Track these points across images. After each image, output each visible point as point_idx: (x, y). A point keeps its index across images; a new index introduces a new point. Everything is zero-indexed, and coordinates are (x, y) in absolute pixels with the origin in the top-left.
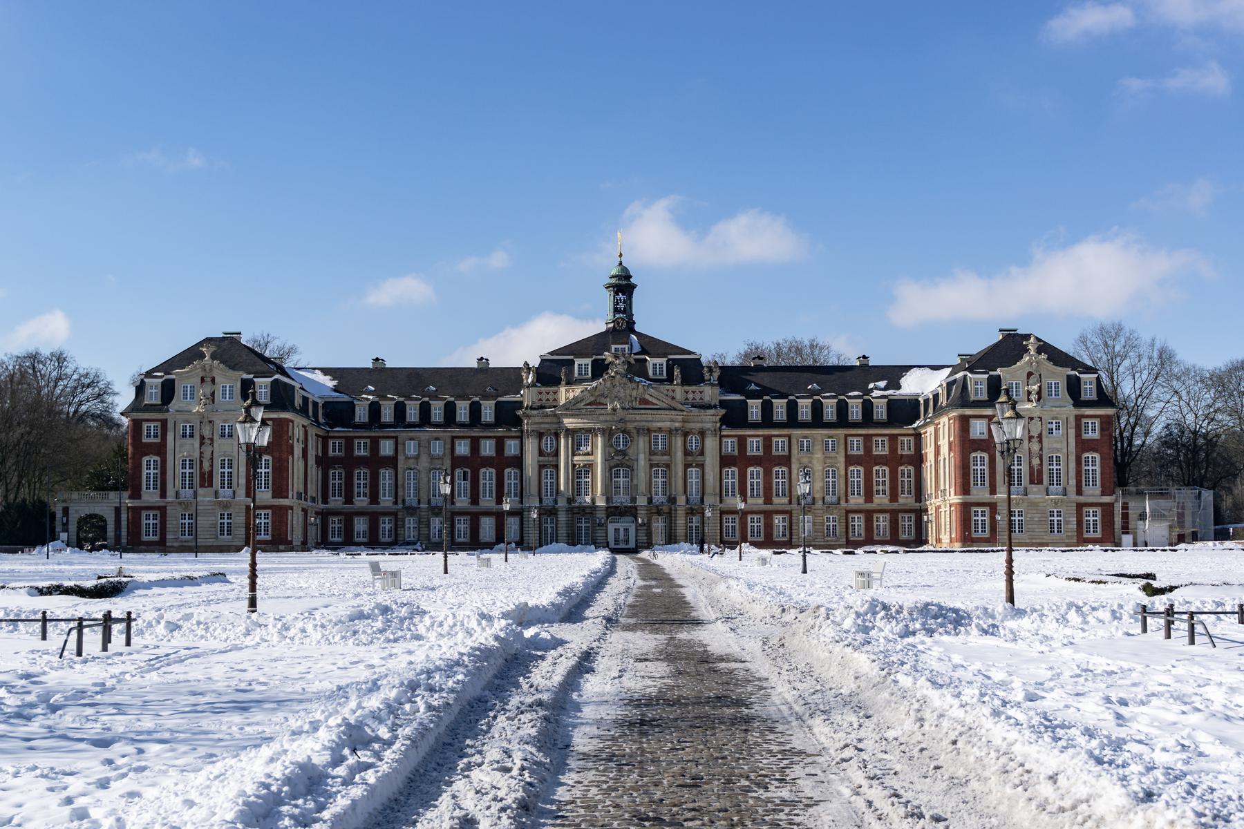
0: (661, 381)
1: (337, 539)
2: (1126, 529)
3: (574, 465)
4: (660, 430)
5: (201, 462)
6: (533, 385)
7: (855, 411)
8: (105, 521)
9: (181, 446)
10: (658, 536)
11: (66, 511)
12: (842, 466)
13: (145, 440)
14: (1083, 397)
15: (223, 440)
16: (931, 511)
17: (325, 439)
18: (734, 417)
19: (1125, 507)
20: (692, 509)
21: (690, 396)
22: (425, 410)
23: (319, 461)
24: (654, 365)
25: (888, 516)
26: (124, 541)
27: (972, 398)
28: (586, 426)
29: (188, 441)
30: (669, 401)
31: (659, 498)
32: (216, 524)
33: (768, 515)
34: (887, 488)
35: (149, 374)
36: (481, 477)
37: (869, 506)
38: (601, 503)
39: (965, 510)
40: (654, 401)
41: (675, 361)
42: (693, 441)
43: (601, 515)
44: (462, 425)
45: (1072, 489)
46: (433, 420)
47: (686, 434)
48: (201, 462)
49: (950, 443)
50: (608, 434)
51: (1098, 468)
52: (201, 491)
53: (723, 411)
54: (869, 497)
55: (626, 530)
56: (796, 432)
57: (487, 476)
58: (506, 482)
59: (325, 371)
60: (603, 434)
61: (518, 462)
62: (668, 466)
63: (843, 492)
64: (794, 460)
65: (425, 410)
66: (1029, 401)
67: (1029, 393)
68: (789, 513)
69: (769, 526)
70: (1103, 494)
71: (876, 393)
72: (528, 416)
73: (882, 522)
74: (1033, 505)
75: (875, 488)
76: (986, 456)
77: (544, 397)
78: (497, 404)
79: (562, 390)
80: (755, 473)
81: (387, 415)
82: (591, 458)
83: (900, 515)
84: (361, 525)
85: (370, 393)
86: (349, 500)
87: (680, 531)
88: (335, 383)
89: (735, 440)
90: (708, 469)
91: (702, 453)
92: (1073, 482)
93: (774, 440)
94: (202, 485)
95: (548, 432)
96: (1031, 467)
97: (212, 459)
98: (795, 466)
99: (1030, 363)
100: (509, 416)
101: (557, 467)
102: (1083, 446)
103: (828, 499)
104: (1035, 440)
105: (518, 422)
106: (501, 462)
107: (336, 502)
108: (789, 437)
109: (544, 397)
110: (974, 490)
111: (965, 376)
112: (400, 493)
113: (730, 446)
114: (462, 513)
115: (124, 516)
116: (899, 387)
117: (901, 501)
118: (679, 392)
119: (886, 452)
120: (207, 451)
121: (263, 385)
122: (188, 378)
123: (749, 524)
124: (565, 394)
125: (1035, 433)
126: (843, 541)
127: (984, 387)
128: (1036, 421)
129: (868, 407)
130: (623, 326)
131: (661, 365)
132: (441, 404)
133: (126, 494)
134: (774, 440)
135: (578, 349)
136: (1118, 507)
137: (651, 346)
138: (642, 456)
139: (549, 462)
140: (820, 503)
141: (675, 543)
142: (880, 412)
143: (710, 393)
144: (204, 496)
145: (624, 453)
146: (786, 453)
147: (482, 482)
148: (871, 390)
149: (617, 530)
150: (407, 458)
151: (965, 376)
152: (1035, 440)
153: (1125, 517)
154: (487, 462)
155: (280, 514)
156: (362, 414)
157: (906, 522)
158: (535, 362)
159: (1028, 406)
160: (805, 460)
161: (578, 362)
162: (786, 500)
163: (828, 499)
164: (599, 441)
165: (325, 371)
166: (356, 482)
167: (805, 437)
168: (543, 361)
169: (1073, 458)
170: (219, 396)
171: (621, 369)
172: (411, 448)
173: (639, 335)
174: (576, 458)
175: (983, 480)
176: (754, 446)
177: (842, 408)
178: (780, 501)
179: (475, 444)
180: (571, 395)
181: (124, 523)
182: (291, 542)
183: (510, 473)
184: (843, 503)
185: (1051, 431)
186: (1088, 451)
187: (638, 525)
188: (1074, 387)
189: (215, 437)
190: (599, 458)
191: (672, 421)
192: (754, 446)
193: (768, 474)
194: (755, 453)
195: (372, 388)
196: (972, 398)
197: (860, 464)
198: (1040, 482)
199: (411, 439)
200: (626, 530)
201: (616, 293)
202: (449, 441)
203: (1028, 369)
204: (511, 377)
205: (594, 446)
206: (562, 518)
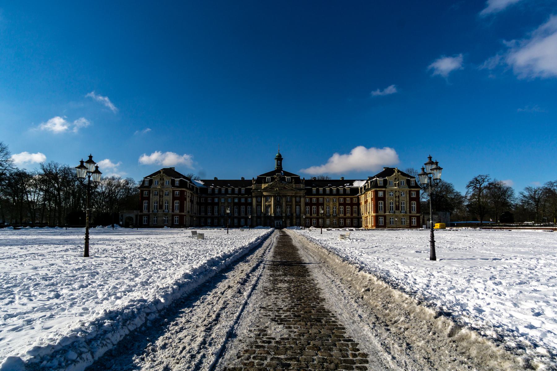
0: (290, 183)
4: (289, 196)
6: (255, 184)
7: (341, 191)
11: (122, 216)
13: (144, 196)
16: (363, 218)
17: (200, 198)
19: (424, 217)
22: (226, 190)
23: (197, 203)
29: (156, 196)
35: (146, 178)
37: (345, 217)
38: (273, 215)
39: (377, 218)
42: (298, 199)
49: (372, 199)
50: (275, 197)
51: (415, 206)
52: (159, 210)
54: (345, 214)
55: (280, 223)
57: (243, 208)
58: (248, 209)
61: (251, 204)
65: (226, 190)
66: (396, 186)
70: (417, 213)
71: (347, 187)
72: (254, 192)
73: (348, 221)
76: (383, 202)
81: (216, 191)
84: (209, 221)
86: (206, 214)
87: (294, 223)
92: (408, 210)
94: (160, 209)
99: (396, 175)
100: (249, 192)
102: (174, 199)
107: (203, 214)
108: (324, 198)
110: (379, 212)
111: (376, 179)
114: (236, 217)
116: (353, 185)
117: (354, 215)
124: (263, 186)
125: (397, 196)
126: (338, 226)
127: (382, 182)
129: (345, 190)
132: (231, 188)
133: (139, 211)
135: (267, 174)
138: (284, 203)
139: (259, 204)
142: (348, 191)
143: (302, 186)
145: (279, 202)
149: (277, 223)
150: (222, 203)
151: (376, 179)
153: (423, 220)
154: (243, 204)
155: (181, 217)
156: (210, 191)
157: (355, 221)
158: (256, 178)
160: (328, 204)
163: (334, 215)
165: (201, 181)
168: (258, 178)
169: (408, 203)
170: (165, 183)
173: (283, 171)
175: (382, 210)
177: (338, 190)
179: (240, 199)
180: (265, 186)
182: (185, 225)
184: (338, 216)
188: (408, 182)
198: (399, 210)
200: (280, 223)
201: (277, 161)
203: (395, 177)
204: (249, 182)
205: (271, 200)
206: (263, 219)
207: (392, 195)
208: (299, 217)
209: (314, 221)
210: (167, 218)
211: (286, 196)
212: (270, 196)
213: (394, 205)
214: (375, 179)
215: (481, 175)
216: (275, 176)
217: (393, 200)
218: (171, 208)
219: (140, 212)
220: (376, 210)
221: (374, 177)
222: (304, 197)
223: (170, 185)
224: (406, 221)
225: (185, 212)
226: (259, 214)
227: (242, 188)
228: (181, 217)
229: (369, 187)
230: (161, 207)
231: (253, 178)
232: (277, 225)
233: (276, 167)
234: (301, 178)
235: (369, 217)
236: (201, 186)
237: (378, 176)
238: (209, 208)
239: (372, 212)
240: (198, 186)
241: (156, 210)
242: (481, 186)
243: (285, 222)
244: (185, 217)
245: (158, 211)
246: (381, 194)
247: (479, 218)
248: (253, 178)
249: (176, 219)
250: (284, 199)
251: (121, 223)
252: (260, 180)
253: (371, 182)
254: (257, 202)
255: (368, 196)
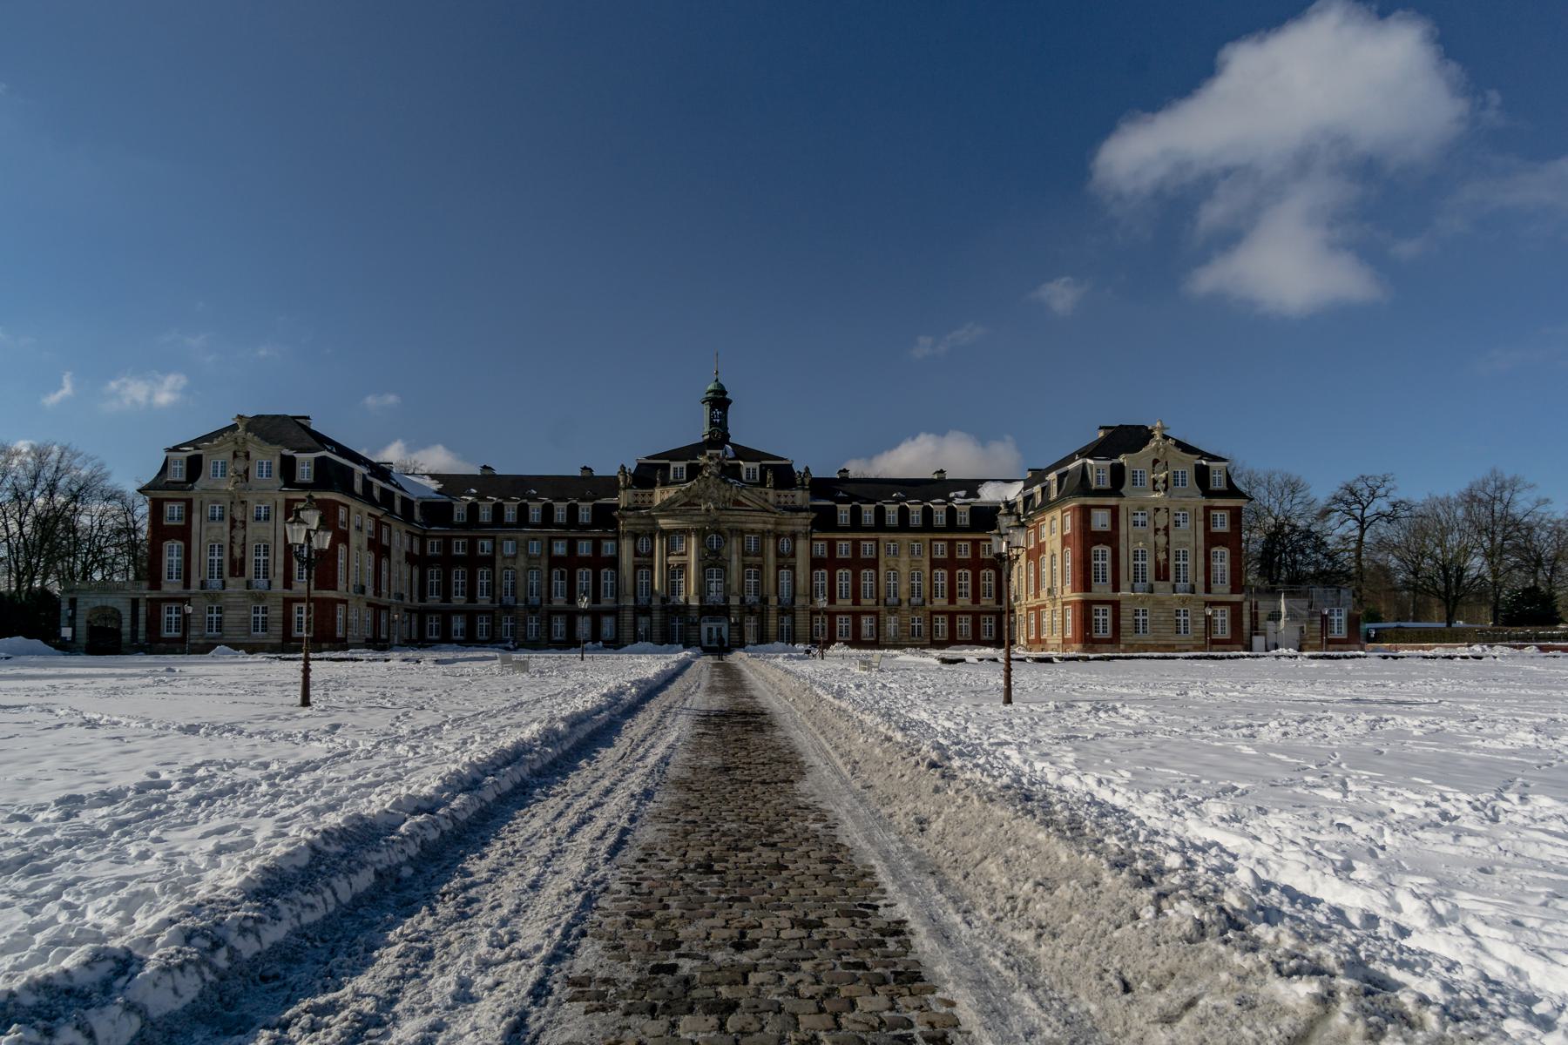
0: (755, 485)
1: (434, 637)
2: (1255, 630)
3: (668, 566)
4: (753, 531)
5: (231, 548)
7: (940, 517)
8: (119, 613)
9: (208, 529)
10: (750, 635)
12: (927, 569)
14: (1212, 487)
15: (257, 524)
16: (1021, 612)
18: (825, 521)
20: (783, 609)
21: (783, 500)
22: (523, 511)
24: (748, 470)
25: (970, 618)
26: (141, 637)
27: (1094, 486)
28: (681, 526)
29: (217, 524)
30: (762, 503)
31: (751, 598)
32: (249, 618)
33: (856, 616)
34: (969, 591)
35: (176, 449)
36: (578, 577)
37: (952, 608)
38: (694, 602)
39: (1086, 611)
40: (748, 503)
41: (768, 466)
42: (785, 544)
43: (694, 614)
44: (559, 526)
45: (1200, 586)
46: (531, 520)
47: (778, 537)
48: (231, 548)
49: (1065, 541)
50: (702, 534)
52: (231, 581)
53: (814, 515)
55: (719, 630)
56: (884, 536)
59: (433, 477)
60: (697, 536)
61: (614, 562)
62: (760, 567)
63: (928, 594)
64: (881, 562)
65: (523, 511)
66: (1156, 490)
67: (1155, 482)
68: (877, 614)
69: (857, 627)
70: (1233, 591)
71: (957, 501)
72: (624, 518)
73: (965, 624)
74: (1159, 603)
75: (958, 591)
76: (1108, 550)
77: (640, 499)
78: (594, 507)
79: (657, 491)
80: (844, 576)
81: (485, 514)
82: (685, 558)
83: (982, 617)
84: (458, 623)
85: (471, 495)
86: (447, 597)
87: (772, 630)
88: (440, 486)
89: (825, 543)
90: (799, 570)
91: (793, 555)
92: (1201, 578)
93: (863, 543)
94: (232, 574)
95: (643, 533)
96: (1157, 563)
97: (244, 544)
98: (882, 569)
99: (1157, 449)
100: (605, 517)
101: (652, 568)
103: (914, 600)
104: (1161, 533)
105: (614, 523)
106: (598, 562)
107: (434, 600)
108: (877, 541)
109: (640, 499)
110: (1095, 586)
111: (1084, 465)
112: (498, 592)
113: (821, 549)
114: (559, 612)
115: (142, 610)
116: (978, 496)
118: (771, 495)
119: (969, 556)
120: (239, 535)
121: (305, 464)
122: (218, 452)
123: (838, 625)
124: (660, 495)
125: (1161, 526)
126: (927, 641)
128: (1162, 511)
129: (951, 513)
130: (719, 436)
131: (754, 470)
134: (863, 543)
135: (675, 455)
136: (1246, 605)
137: (744, 453)
138: (735, 557)
139: (644, 562)
140: (905, 605)
141: (767, 642)
142: (964, 518)
143: (800, 497)
144: (234, 587)
145: (717, 553)
146: (873, 556)
147: (578, 582)
148: (953, 499)
149: (710, 630)
150: (505, 558)
151: (1084, 465)
152: (1161, 533)
153: (1254, 617)
154: (584, 562)
155: (324, 611)
157: (988, 623)
158: (632, 467)
159: (1156, 495)
160: (892, 564)
161: (673, 465)
162: (873, 602)
164: (693, 540)
165: (433, 477)
166: (454, 580)
167: (892, 541)
168: (640, 465)
169: (1201, 553)
171: (715, 470)
172: (509, 546)
173: (733, 445)
174: (670, 558)
176: (844, 550)
177: (928, 513)
178: (868, 602)
179: (572, 545)
180: (666, 496)
181: (142, 617)
183: (867, 573)
184: (928, 605)
185: (1177, 524)
186: (1216, 545)
187: (730, 625)
188: (1202, 475)
189: (249, 520)
190: (692, 558)
191: (765, 522)
192: (844, 550)
193: (856, 577)
194: (844, 556)
195: (474, 491)
196: (1094, 486)
197: (944, 568)
198: (1167, 578)
199: (510, 539)
200: (719, 630)
201: (712, 409)
202: (546, 541)
203: (1154, 456)
204: (609, 485)
206: (657, 617)
207: (1144, 524)
208: (787, 610)
209: (843, 623)
210: (265, 610)
211: (741, 533)
212: (685, 532)
213: (1150, 564)
214: (1080, 462)
215: (1367, 474)
216: (702, 460)
217: (1146, 541)
218: (280, 570)
219: (151, 588)
220: (1085, 580)
221: (1071, 459)
222: (807, 535)
223: (277, 481)
224: (1195, 623)
225: (341, 585)
226: (643, 600)
227: (582, 505)
228: (324, 611)
229: (1054, 495)
230: (238, 568)
231: (623, 467)
232: (710, 640)
233: (707, 429)
234: (798, 468)
235: (1050, 607)
236: (426, 494)
237: (1093, 451)
238: (458, 578)
239: (1068, 591)
240: (414, 495)
241: (216, 582)
242: (1367, 512)
243: (740, 627)
244: (340, 606)
245: (224, 584)
246: (1101, 520)
247: (1437, 610)
248: (623, 467)
249: (301, 613)
250: (735, 544)
251: (66, 632)
252: (647, 475)
253: (1061, 477)
254: (637, 554)
255: (1045, 530)
